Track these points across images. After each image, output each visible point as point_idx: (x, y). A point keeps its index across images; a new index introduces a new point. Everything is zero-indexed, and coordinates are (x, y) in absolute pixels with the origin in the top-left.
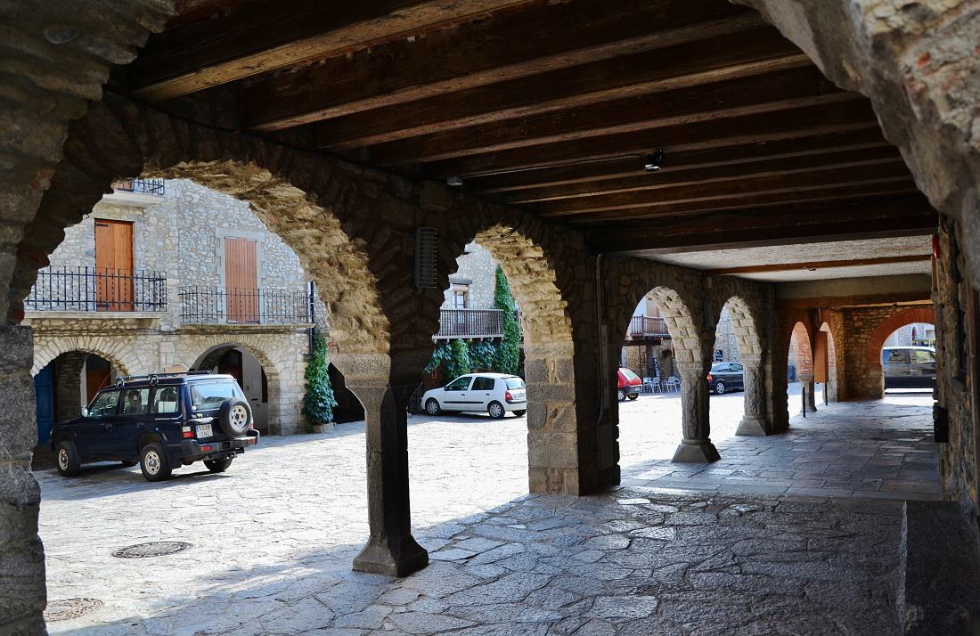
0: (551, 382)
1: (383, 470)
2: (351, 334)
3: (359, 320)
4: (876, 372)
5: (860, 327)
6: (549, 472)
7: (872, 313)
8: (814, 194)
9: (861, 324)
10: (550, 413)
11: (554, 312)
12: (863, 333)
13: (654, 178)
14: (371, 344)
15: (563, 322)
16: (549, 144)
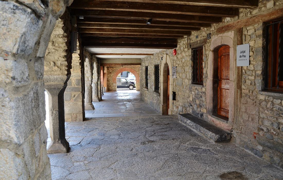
0: (73, 86)
1: (59, 117)
2: (50, 68)
3: (55, 63)
4: (115, 84)
5: (111, 72)
6: (72, 115)
7: (114, 68)
8: (155, 35)
9: (111, 71)
10: (73, 96)
11: (76, 64)
12: (112, 73)
13: (148, 26)
14: (59, 72)
15: (78, 67)
16: (119, 11)
